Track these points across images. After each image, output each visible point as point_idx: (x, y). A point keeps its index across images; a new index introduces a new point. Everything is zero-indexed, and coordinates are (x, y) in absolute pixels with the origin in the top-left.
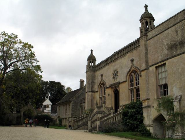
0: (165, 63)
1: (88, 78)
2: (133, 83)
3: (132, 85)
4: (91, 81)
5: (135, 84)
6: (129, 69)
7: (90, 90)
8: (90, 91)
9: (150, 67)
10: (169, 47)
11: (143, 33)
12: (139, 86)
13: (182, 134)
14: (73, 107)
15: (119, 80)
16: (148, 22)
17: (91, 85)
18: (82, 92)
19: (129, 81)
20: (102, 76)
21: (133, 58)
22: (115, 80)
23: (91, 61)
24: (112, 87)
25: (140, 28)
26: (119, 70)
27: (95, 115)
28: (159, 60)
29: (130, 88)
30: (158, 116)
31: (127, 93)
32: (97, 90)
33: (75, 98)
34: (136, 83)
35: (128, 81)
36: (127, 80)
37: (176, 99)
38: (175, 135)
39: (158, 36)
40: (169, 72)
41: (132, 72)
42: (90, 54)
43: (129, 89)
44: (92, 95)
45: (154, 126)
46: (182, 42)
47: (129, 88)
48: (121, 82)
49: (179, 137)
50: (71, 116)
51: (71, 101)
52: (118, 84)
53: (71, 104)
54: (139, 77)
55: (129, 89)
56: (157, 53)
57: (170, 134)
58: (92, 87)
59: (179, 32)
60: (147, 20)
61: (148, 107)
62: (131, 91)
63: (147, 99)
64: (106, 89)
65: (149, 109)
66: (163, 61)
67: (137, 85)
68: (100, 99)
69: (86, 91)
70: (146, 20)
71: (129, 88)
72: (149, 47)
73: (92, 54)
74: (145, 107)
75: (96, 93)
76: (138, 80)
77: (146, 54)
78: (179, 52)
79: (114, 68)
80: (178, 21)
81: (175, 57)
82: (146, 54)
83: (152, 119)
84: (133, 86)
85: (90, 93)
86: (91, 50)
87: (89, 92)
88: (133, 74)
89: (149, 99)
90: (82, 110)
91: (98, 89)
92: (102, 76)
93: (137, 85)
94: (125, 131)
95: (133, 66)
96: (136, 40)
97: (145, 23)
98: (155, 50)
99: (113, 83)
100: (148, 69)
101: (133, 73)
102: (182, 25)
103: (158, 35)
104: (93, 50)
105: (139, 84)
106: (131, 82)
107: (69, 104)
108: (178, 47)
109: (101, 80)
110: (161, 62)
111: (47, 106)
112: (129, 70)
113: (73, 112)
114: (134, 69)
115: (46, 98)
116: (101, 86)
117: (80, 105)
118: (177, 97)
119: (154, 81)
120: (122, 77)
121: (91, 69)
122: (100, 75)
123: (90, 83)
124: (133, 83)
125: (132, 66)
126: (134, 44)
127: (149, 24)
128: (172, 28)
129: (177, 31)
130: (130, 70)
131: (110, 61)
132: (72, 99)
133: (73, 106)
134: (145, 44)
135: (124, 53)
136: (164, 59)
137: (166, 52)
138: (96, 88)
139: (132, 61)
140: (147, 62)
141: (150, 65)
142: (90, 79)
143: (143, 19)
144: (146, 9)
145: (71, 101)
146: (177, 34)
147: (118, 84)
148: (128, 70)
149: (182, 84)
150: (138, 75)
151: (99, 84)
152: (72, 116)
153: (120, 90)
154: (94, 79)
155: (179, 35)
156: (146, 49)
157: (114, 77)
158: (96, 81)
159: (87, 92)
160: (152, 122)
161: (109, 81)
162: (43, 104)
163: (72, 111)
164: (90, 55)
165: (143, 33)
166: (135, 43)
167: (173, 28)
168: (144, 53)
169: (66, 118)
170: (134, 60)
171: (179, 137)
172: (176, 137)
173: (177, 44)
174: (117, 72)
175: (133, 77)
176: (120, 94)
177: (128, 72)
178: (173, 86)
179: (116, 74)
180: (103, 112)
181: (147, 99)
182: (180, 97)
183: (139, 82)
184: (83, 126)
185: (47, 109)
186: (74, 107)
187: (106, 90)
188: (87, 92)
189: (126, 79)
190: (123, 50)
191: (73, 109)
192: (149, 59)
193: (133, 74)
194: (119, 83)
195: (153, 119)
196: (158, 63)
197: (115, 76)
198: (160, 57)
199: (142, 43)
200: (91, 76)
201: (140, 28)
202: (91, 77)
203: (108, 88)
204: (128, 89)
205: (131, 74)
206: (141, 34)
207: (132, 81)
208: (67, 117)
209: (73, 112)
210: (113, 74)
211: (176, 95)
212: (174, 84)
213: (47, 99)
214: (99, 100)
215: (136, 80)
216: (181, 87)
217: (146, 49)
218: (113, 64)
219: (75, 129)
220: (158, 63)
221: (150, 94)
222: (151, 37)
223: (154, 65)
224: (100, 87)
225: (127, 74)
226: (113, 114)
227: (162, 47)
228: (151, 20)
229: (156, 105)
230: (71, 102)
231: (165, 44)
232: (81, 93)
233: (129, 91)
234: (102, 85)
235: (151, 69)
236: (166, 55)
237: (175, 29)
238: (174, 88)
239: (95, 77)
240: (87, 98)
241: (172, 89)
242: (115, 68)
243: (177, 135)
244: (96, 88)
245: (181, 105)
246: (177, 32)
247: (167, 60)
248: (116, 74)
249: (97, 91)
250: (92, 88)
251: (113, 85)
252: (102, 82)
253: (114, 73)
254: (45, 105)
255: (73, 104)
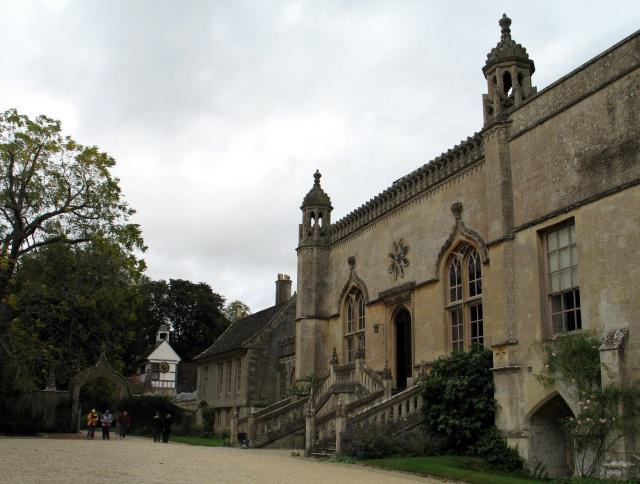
0: (572, 219)
1: (303, 269)
2: (460, 288)
3: (456, 294)
4: (315, 279)
5: (467, 290)
6: (447, 238)
7: (312, 313)
8: (312, 313)
9: (519, 230)
10: (583, 163)
11: (495, 115)
12: (480, 299)
13: (630, 464)
14: (253, 369)
15: (410, 275)
16: (512, 77)
17: (314, 295)
18: (282, 318)
19: (445, 279)
20: (352, 261)
21: (462, 200)
22: (399, 277)
23: (315, 211)
24: (387, 300)
25: (484, 95)
26: (410, 242)
27: (328, 397)
28: (552, 208)
29: (450, 304)
30: (545, 401)
31: (440, 320)
32: (334, 311)
33: (258, 340)
34: (472, 285)
35: (441, 280)
36: (441, 276)
37: (608, 343)
38: (607, 468)
39: (547, 124)
40: (585, 249)
41: (456, 250)
42: (312, 187)
43: (447, 309)
44: (317, 330)
45: (533, 437)
46: (630, 145)
47: (446, 304)
48: (418, 283)
49: (618, 473)
50: (244, 402)
51: (247, 349)
52: (407, 290)
53: (246, 361)
54: (482, 265)
55: (447, 309)
56: (542, 184)
57: (588, 464)
58: (320, 301)
59: (618, 110)
60: (508, 69)
61: (512, 369)
62: (454, 315)
63: (508, 344)
64: (366, 308)
65: (516, 376)
66: (564, 211)
67: (472, 294)
68: (346, 343)
69: (298, 316)
70: (505, 70)
71: (446, 304)
72: (514, 162)
73: (319, 186)
74: (503, 370)
75: (333, 323)
76: (479, 275)
77: (507, 185)
78: (618, 181)
79: (395, 235)
80: (617, 73)
81: (606, 199)
82: (507, 185)
83: (527, 411)
84: (460, 298)
85: (311, 323)
86: (315, 172)
87: (310, 318)
88: (460, 256)
89: (514, 344)
90: (285, 379)
91: (339, 309)
92: (352, 261)
93: (472, 294)
94: (431, 454)
95: (461, 229)
96: (469, 138)
97: (502, 79)
98: (535, 174)
99: (389, 286)
100: (513, 239)
101: (462, 252)
102: (629, 87)
103: (546, 119)
104: (320, 172)
105: (480, 292)
106: (453, 283)
107: (239, 360)
108: (617, 161)
109: (350, 278)
110: (556, 214)
111: (162, 367)
112: (447, 242)
113: (252, 388)
114: (463, 238)
115: (158, 338)
116: (348, 297)
117: (278, 362)
118: (611, 336)
119: (531, 279)
120: (421, 267)
121: (315, 237)
122: (346, 258)
123: (312, 286)
124: (460, 288)
125: (456, 228)
126: (465, 153)
127: (514, 81)
128: (596, 96)
129: (614, 109)
130: (449, 243)
131: (379, 210)
132: (251, 342)
133: (251, 365)
134: (501, 153)
135: (430, 184)
136: (566, 204)
137: (574, 179)
138: (332, 304)
139: (457, 209)
140: (508, 215)
141: (518, 223)
142: (311, 273)
143: (494, 67)
144: (506, 31)
145: (247, 349)
146: (614, 119)
147: (407, 290)
148: (442, 241)
149: (628, 292)
150: (478, 260)
151: (344, 291)
152: (248, 401)
153: (416, 310)
154: (327, 274)
155: (620, 121)
156: (506, 171)
157: (393, 267)
158: (333, 281)
159: (300, 320)
160: (526, 421)
161: (377, 279)
162: (149, 358)
163: (251, 383)
164: (312, 191)
165: (495, 115)
166: (466, 149)
167: (599, 98)
168: (500, 182)
169: (228, 409)
170: (464, 207)
171: (618, 473)
172: (610, 473)
173: (613, 151)
174: (406, 250)
175: (459, 268)
176: (416, 327)
177: (444, 249)
178: (599, 297)
179: (400, 256)
180: (357, 389)
181: (508, 344)
182: (621, 335)
183: (479, 283)
184: (289, 437)
185: (163, 376)
186: (257, 368)
187: (367, 310)
188: (300, 320)
189: (437, 272)
190: (424, 175)
191: (253, 378)
192: (515, 206)
193: (460, 256)
194: (413, 287)
195: (530, 412)
196: (546, 218)
197: (399, 261)
198: (554, 199)
199: (491, 148)
200: (314, 262)
201: (484, 95)
202: (315, 265)
203: (373, 303)
204: (442, 307)
205: (451, 255)
206: (486, 118)
207: (455, 280)
208: (230, 403)
209: (252, 388)
210: (392, 256)
211: (608, 328)
212: (603, 292)
213: (161, 343)
214: (343, 347)
215: (471, 277)
216: (627, 302)
217: (506, 171)
218: (392, 220)
219: (260, 447)
220: (546, 218)
221: (520, 324)
222: (522, 128)
223: (533, 224)
224: (346, 301)
225: (440, 256)
226: (390, 394)
227: (561, 162)
228: (522, 70)
229: (538, 364)
230: (245, 351)
231: (572, 152)
232: (282, 321)
233: (445, 315)
234: (351, 292)
235: (523, 238)
236: (574, 189)
237: (605, 100)
238: (604, 305)
239: (327, 267)
240: (302, 340)
241: (596, 306)
242: (397, 235)
243: (613, 468)
244: (332, 304)
245: (625, 363)
246: (611, 110)
247: (579, 206)
248: (400, 256)
249: (336, 316)
250: (317, 305)
251: (393, 292)
252: (353, 284)
253: (393, 252)
254: (157, 364)
255: (252, 358)
